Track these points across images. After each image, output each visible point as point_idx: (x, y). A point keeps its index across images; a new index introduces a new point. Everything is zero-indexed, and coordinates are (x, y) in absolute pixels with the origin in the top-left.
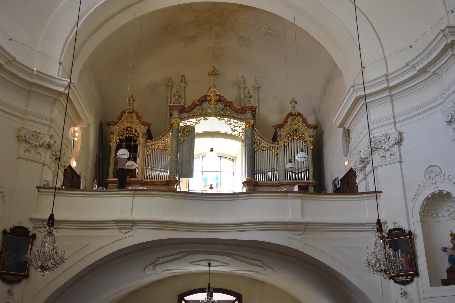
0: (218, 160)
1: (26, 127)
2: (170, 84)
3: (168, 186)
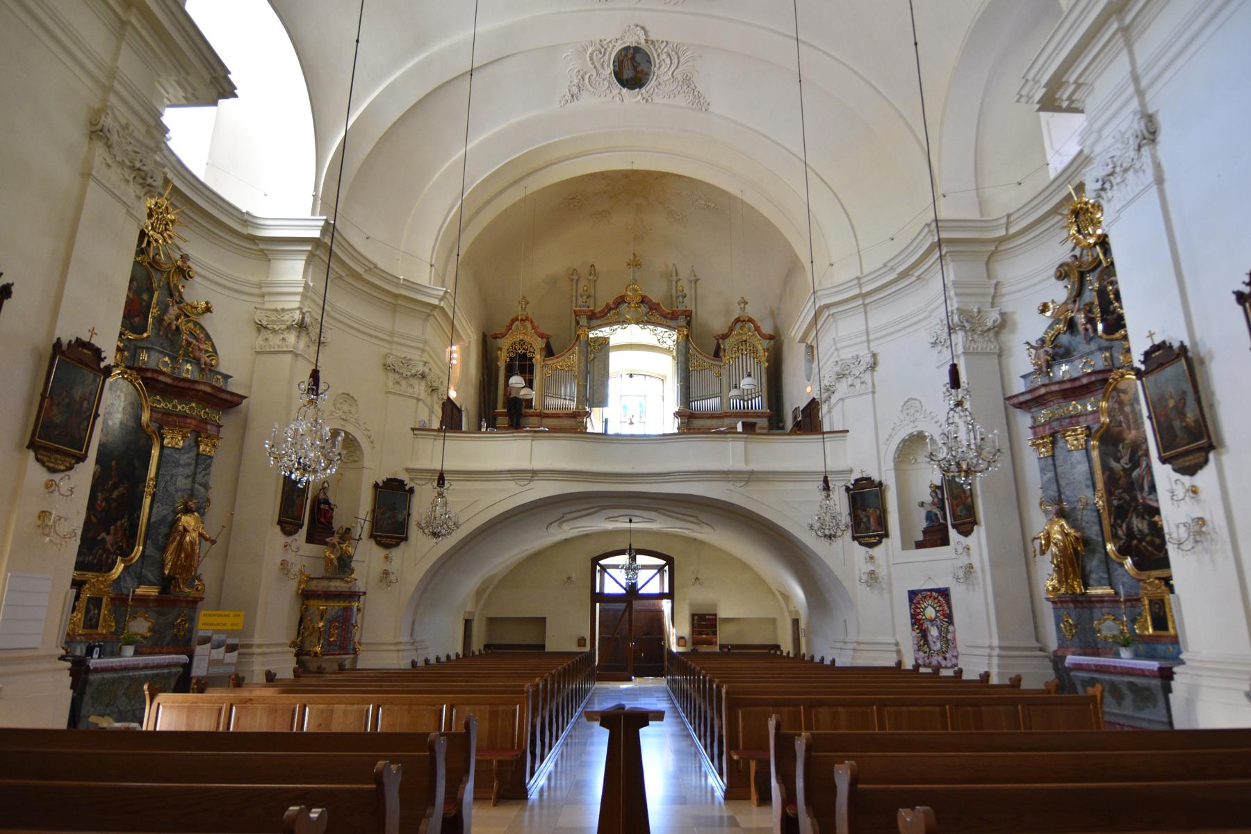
0: (641, 385)
1: (394, 352)
2: (575, 277)
3: (572, 424)
